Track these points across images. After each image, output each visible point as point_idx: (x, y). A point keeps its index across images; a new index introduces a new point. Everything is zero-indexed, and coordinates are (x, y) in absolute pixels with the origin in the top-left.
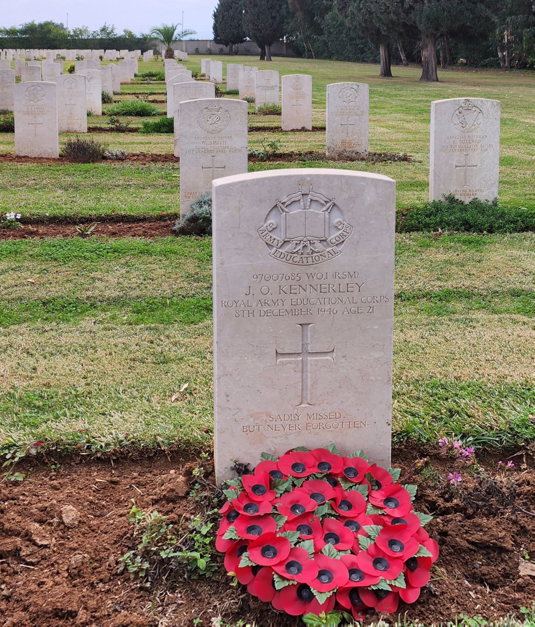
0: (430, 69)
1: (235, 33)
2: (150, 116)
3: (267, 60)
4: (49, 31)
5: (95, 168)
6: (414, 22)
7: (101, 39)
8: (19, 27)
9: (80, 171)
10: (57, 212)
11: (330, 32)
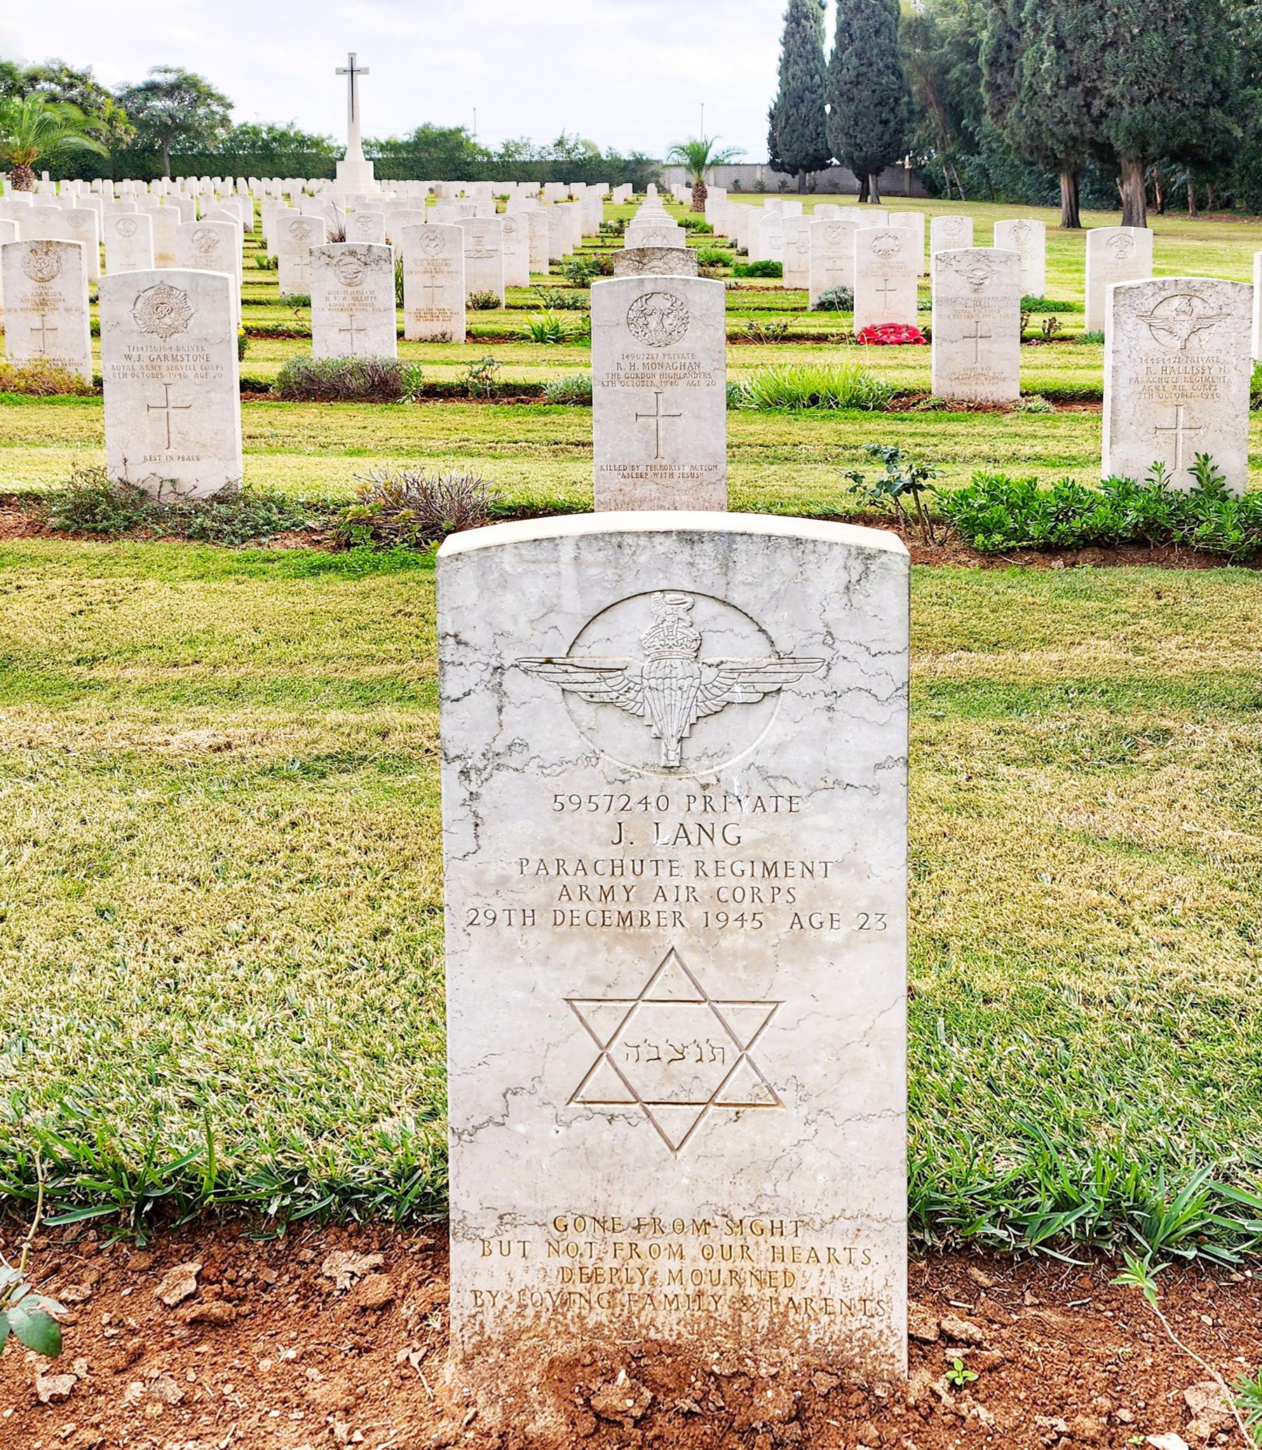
0: (1134, 214)
1: (811, 150)
3: (872, 202)
4: (460, 146)
6: (1108, 138)
11: (992, 150)
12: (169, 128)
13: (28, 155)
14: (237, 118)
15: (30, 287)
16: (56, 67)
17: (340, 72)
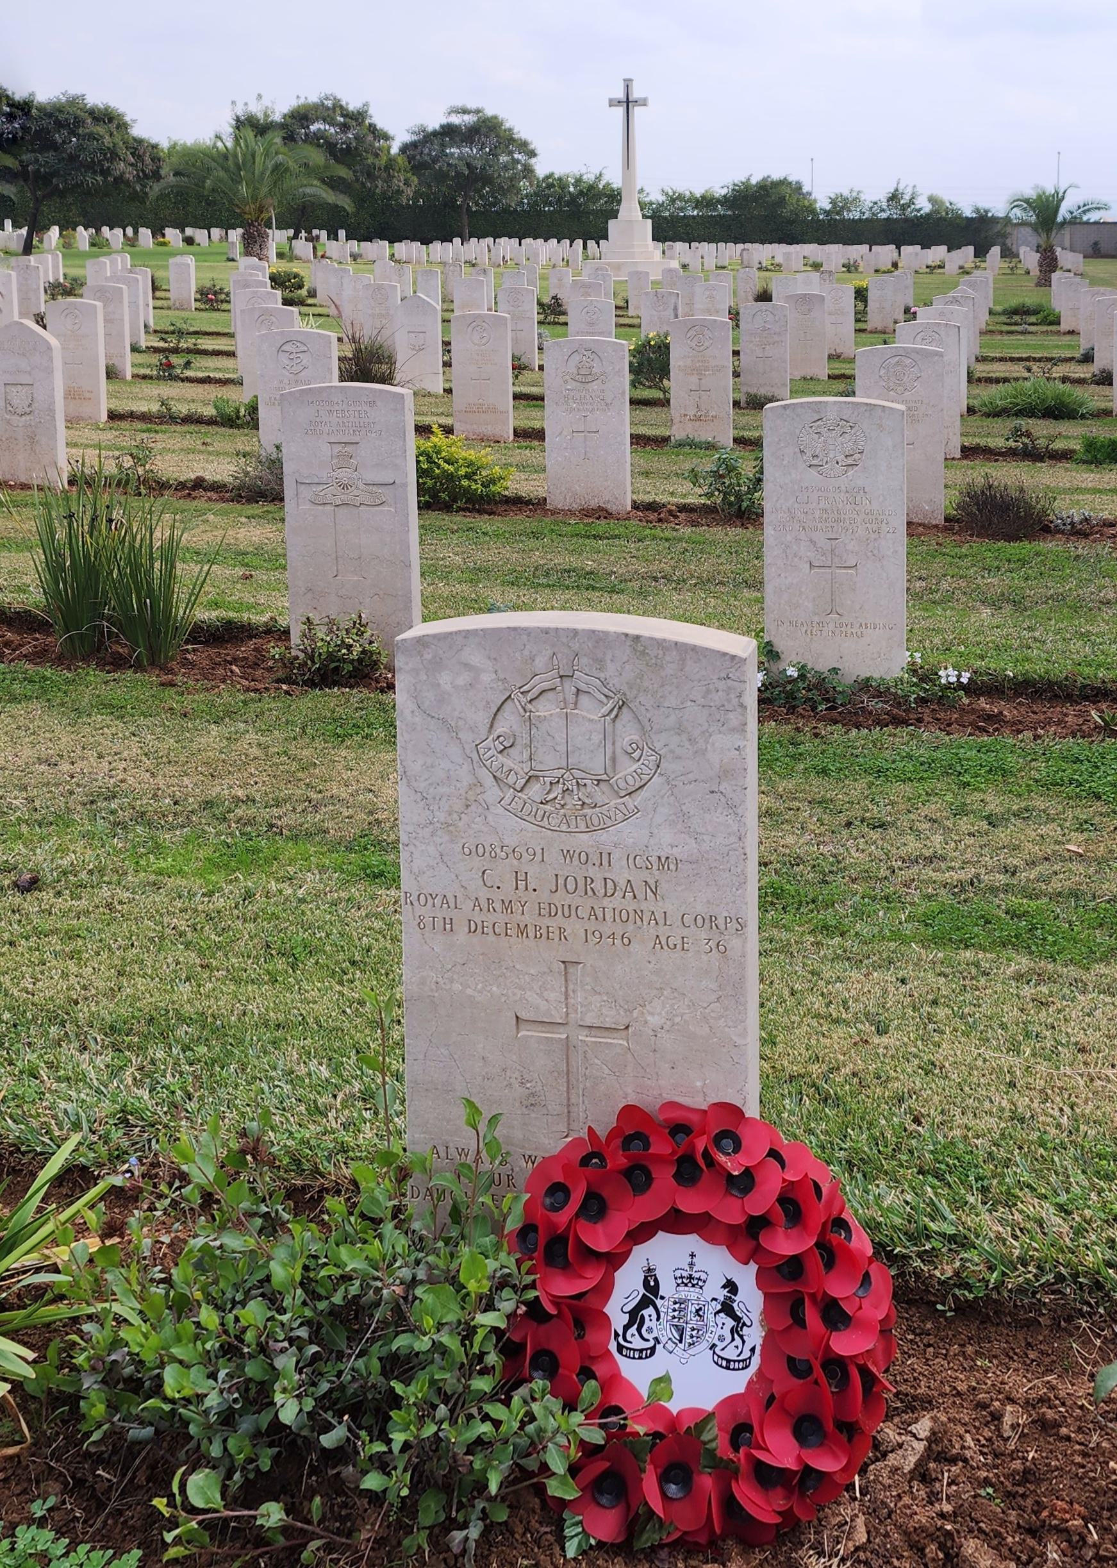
2: (1074, 418)
4: (782, 201)
5: (1038, 554)
7: (888, 219)
8: (720, 192)
9: (1009, 561)
10: (1037, 669)
12: (475, 178)
14: (542, 167)
16: (329, 103)
17: (613, 103)
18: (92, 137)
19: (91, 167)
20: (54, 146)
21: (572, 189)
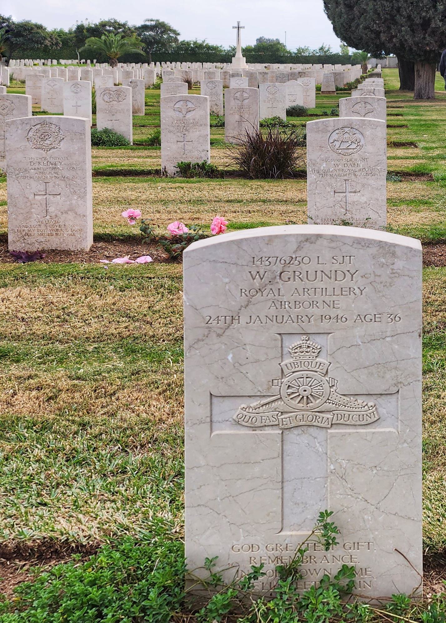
4: (278, 50)
12: (149, 42)
13: (117, 54)
14: (181, 39)
15: (223, 77)
16: (112, 21)
18: (38, 33)
19: (37, 42)
20: (23, 36)
21: (192, 45)
